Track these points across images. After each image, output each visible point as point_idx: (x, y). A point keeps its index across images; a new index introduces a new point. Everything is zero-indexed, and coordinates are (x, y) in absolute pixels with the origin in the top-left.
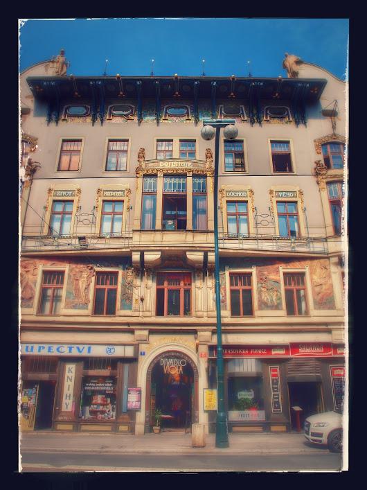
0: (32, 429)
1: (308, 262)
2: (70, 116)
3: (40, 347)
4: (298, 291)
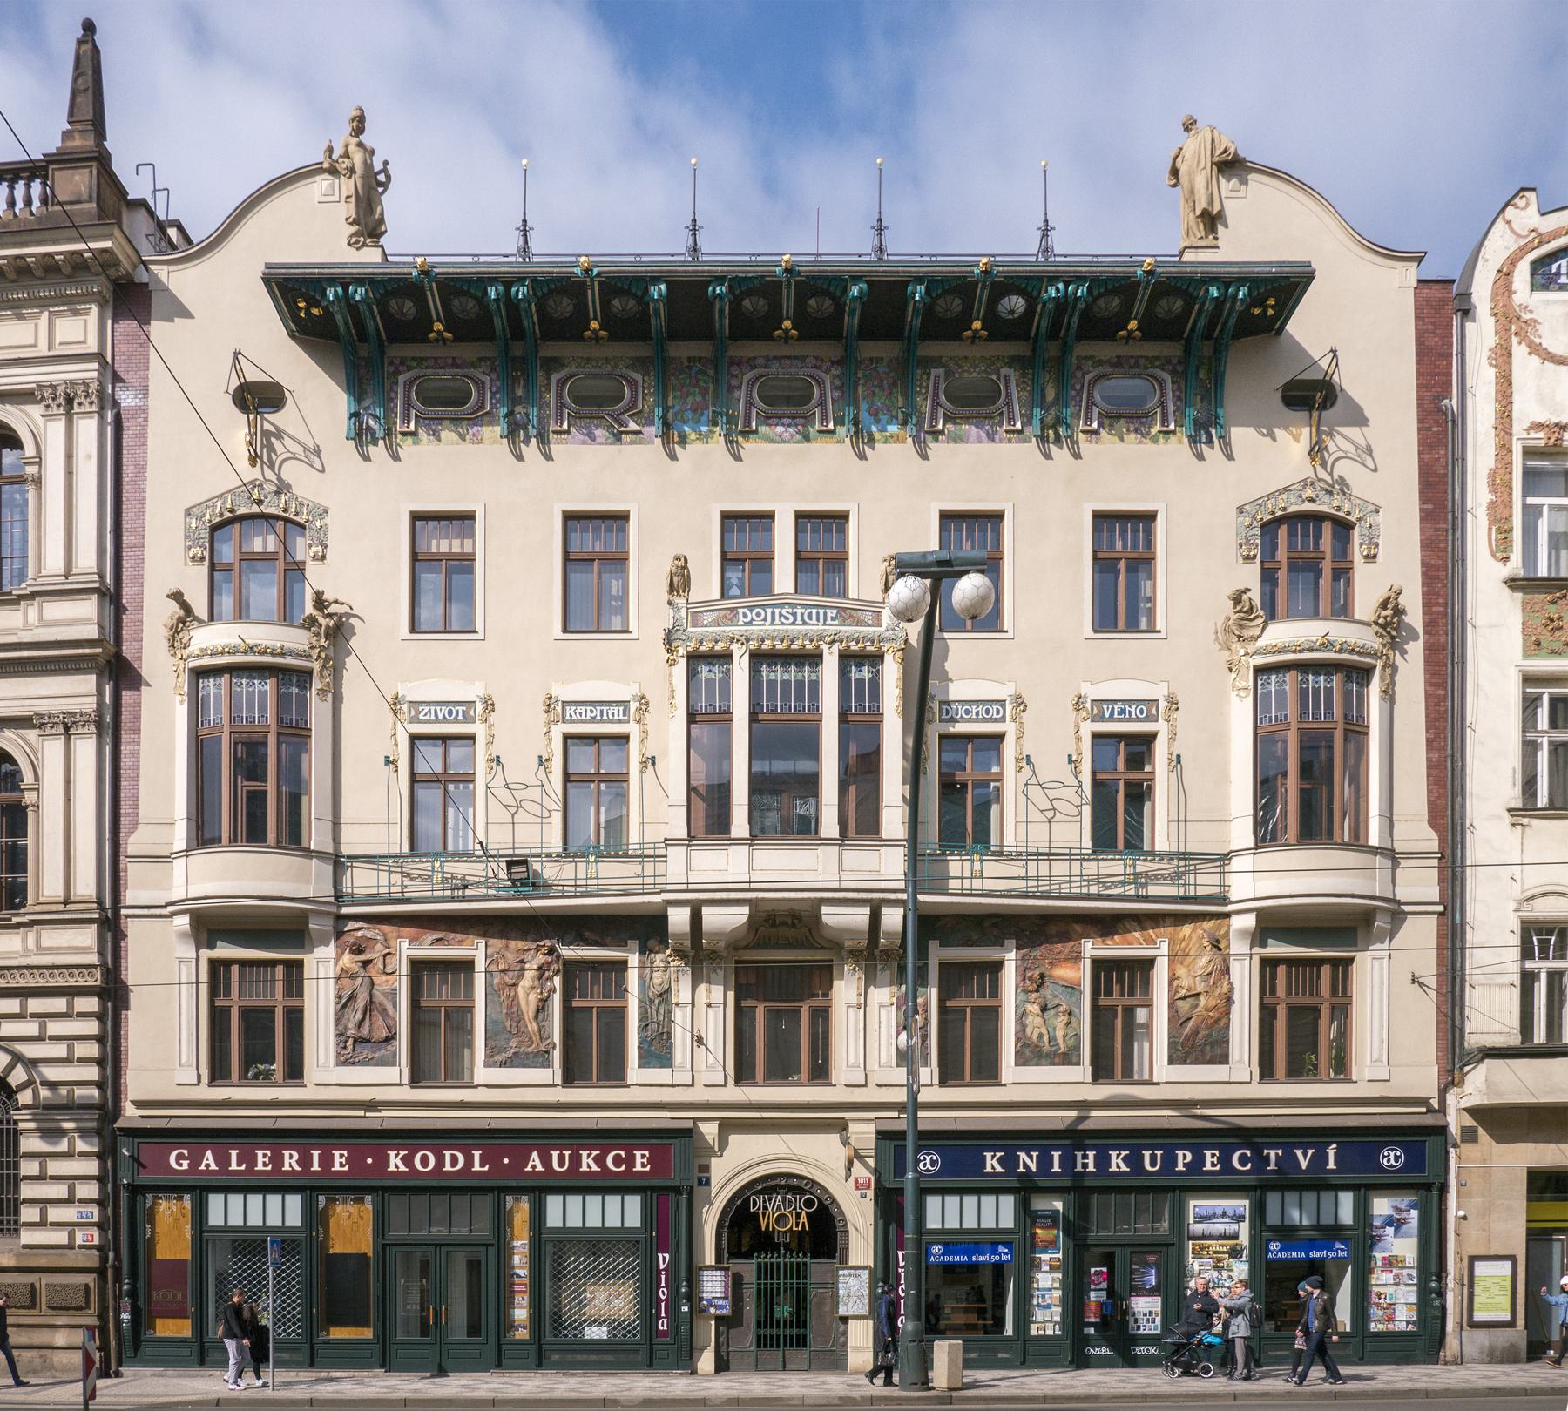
4: (1129, 1011)
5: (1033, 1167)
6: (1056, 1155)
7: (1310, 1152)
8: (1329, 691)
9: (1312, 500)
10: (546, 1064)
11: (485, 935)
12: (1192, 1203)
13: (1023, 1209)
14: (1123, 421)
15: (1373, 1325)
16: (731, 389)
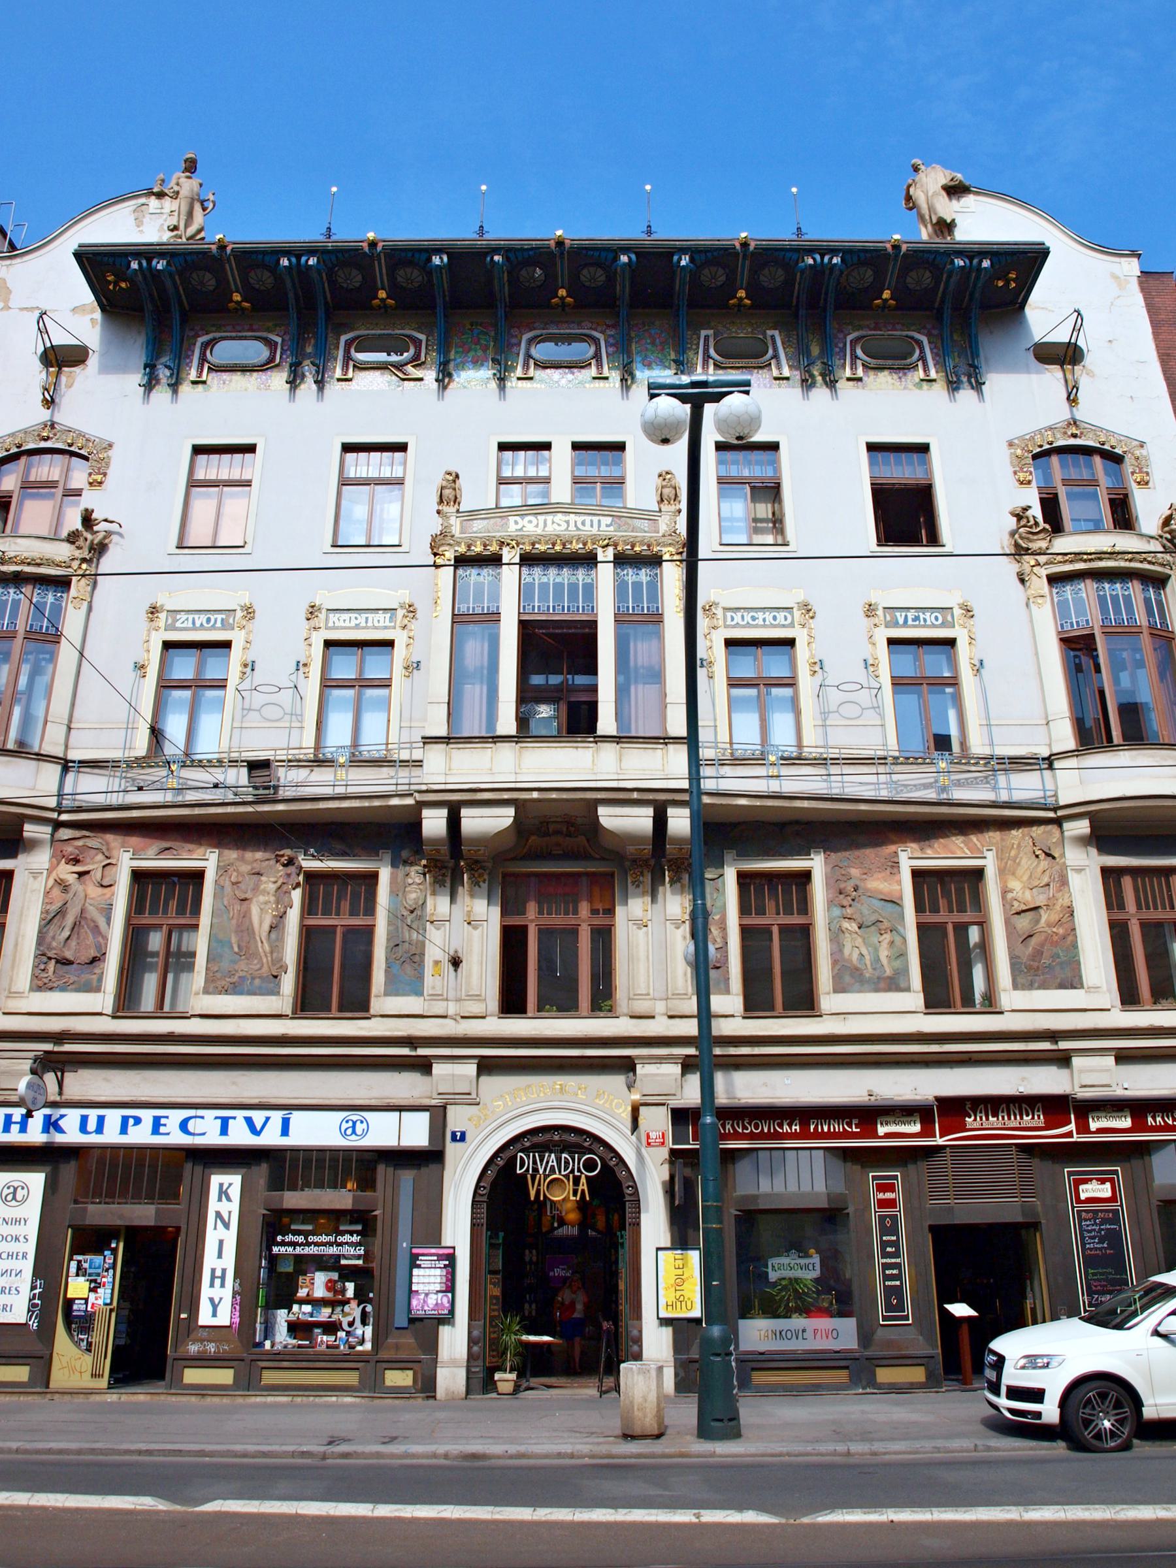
0: (103, 1383)
1: (994, 836)
2: (216, 369)
3: (125, 1120)
4: (961, 929)
8: (1127, 599)
9: (1074, 436)
16: (510, 346)
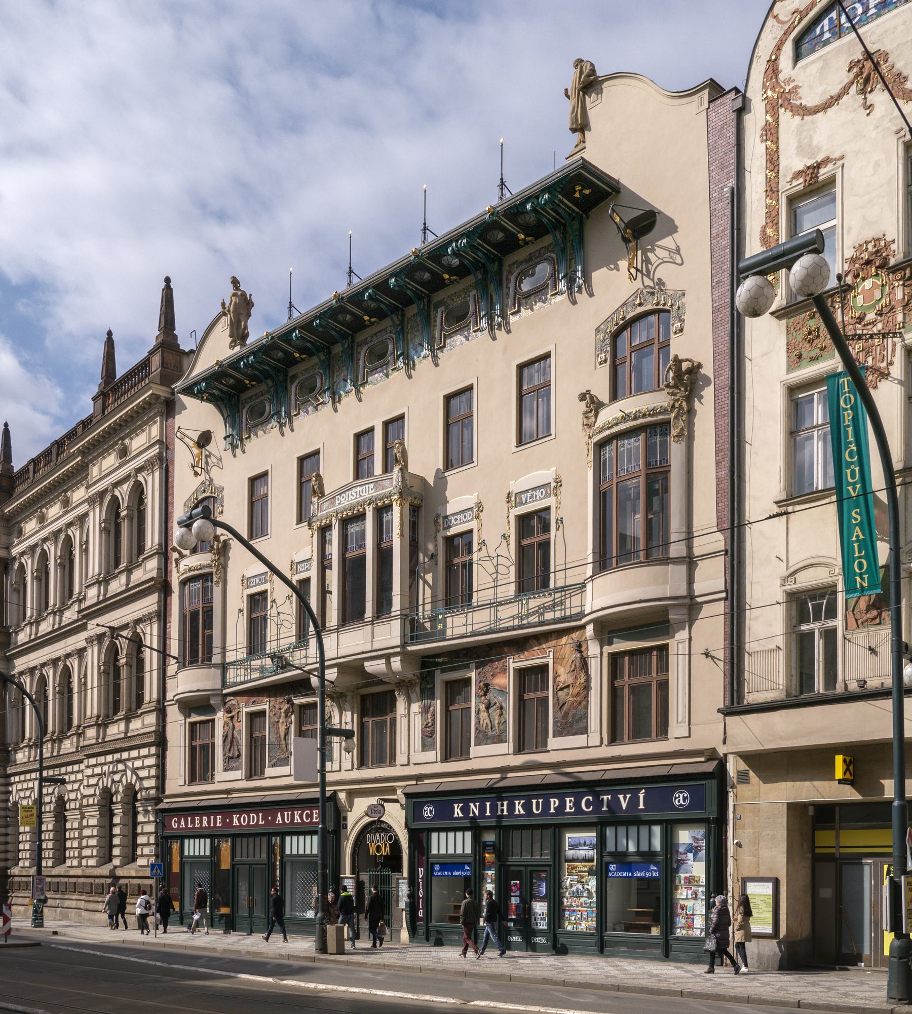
5: (477, 812)
6: (488, 804)
7: (628, 796)
9: (640, 305)
10: (287, 764)
11: (269, 696)
12: (568, 835)
13: (476, 840)
14: (532, 297)
15: (678, 931)
